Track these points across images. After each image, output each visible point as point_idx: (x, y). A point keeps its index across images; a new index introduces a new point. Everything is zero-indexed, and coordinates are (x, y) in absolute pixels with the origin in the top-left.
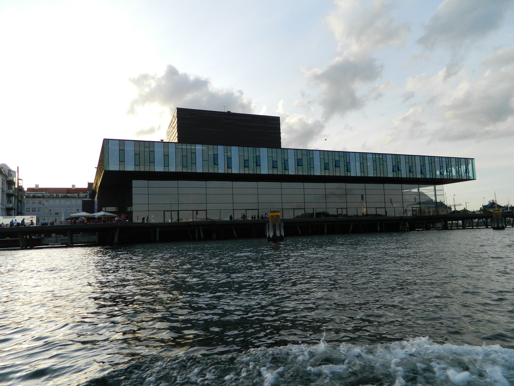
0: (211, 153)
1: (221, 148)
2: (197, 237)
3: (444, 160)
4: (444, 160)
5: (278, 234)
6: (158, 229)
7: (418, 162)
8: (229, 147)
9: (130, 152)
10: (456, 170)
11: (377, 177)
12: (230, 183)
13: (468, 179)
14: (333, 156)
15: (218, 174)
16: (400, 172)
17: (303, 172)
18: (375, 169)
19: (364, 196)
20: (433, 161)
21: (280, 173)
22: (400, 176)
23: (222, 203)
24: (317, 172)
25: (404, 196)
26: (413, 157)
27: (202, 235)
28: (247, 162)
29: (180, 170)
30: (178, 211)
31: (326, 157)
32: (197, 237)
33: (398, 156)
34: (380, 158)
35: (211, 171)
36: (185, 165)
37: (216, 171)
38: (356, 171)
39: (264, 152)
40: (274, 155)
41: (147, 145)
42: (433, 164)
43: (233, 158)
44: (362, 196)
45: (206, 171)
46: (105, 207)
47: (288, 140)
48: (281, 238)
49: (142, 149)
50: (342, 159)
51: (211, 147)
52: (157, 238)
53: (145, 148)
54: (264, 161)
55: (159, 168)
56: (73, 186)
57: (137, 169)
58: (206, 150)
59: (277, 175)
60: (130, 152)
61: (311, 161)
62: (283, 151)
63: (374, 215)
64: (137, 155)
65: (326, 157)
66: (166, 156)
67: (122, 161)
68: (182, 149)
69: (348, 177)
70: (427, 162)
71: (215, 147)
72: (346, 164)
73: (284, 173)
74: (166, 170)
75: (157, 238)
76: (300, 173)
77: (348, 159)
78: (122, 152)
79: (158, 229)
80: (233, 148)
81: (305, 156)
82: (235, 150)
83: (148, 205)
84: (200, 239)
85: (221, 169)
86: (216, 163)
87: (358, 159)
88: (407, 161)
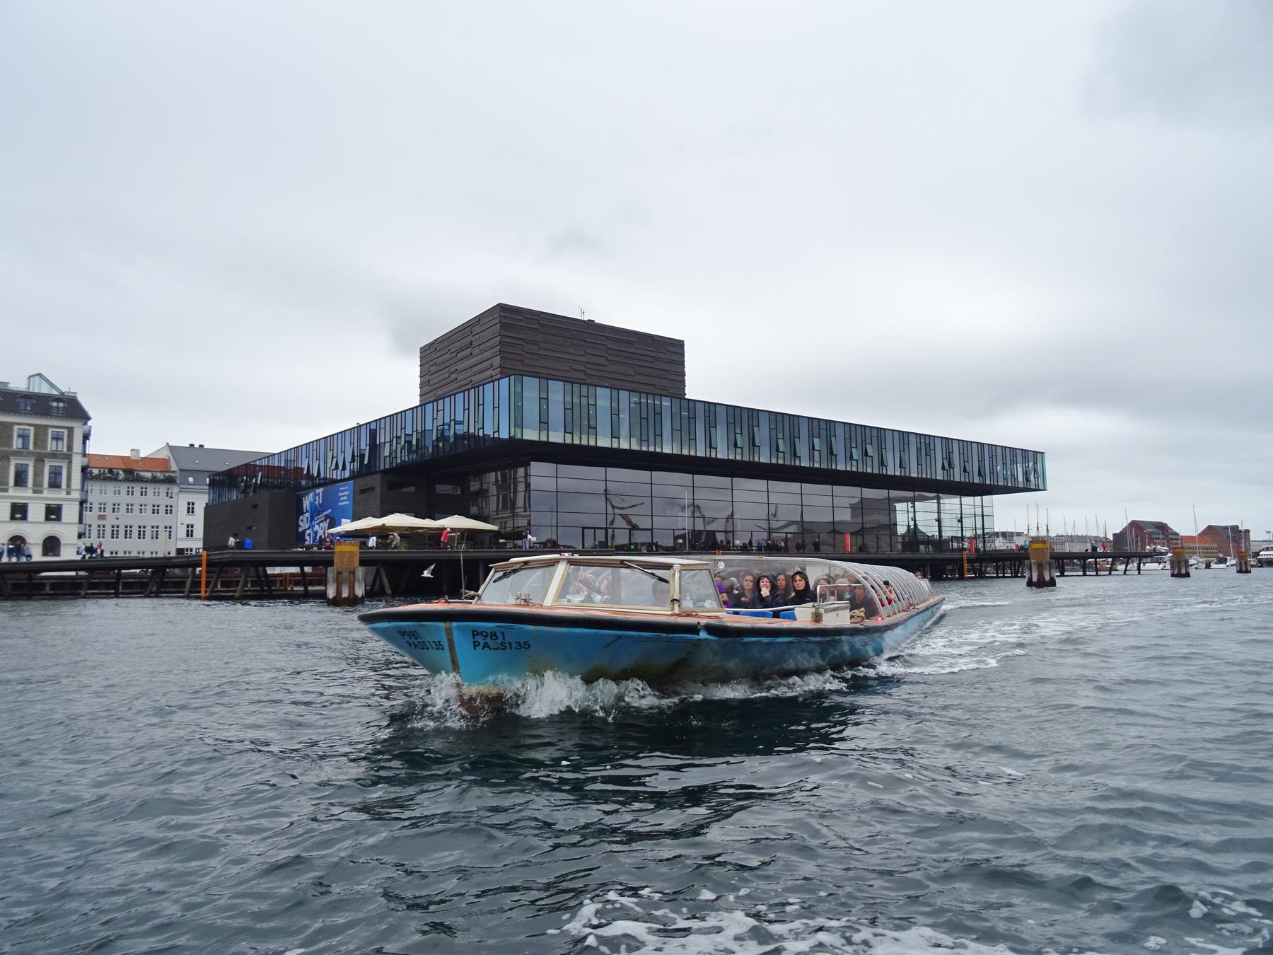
47: (698, 387)
67: (544, 423)
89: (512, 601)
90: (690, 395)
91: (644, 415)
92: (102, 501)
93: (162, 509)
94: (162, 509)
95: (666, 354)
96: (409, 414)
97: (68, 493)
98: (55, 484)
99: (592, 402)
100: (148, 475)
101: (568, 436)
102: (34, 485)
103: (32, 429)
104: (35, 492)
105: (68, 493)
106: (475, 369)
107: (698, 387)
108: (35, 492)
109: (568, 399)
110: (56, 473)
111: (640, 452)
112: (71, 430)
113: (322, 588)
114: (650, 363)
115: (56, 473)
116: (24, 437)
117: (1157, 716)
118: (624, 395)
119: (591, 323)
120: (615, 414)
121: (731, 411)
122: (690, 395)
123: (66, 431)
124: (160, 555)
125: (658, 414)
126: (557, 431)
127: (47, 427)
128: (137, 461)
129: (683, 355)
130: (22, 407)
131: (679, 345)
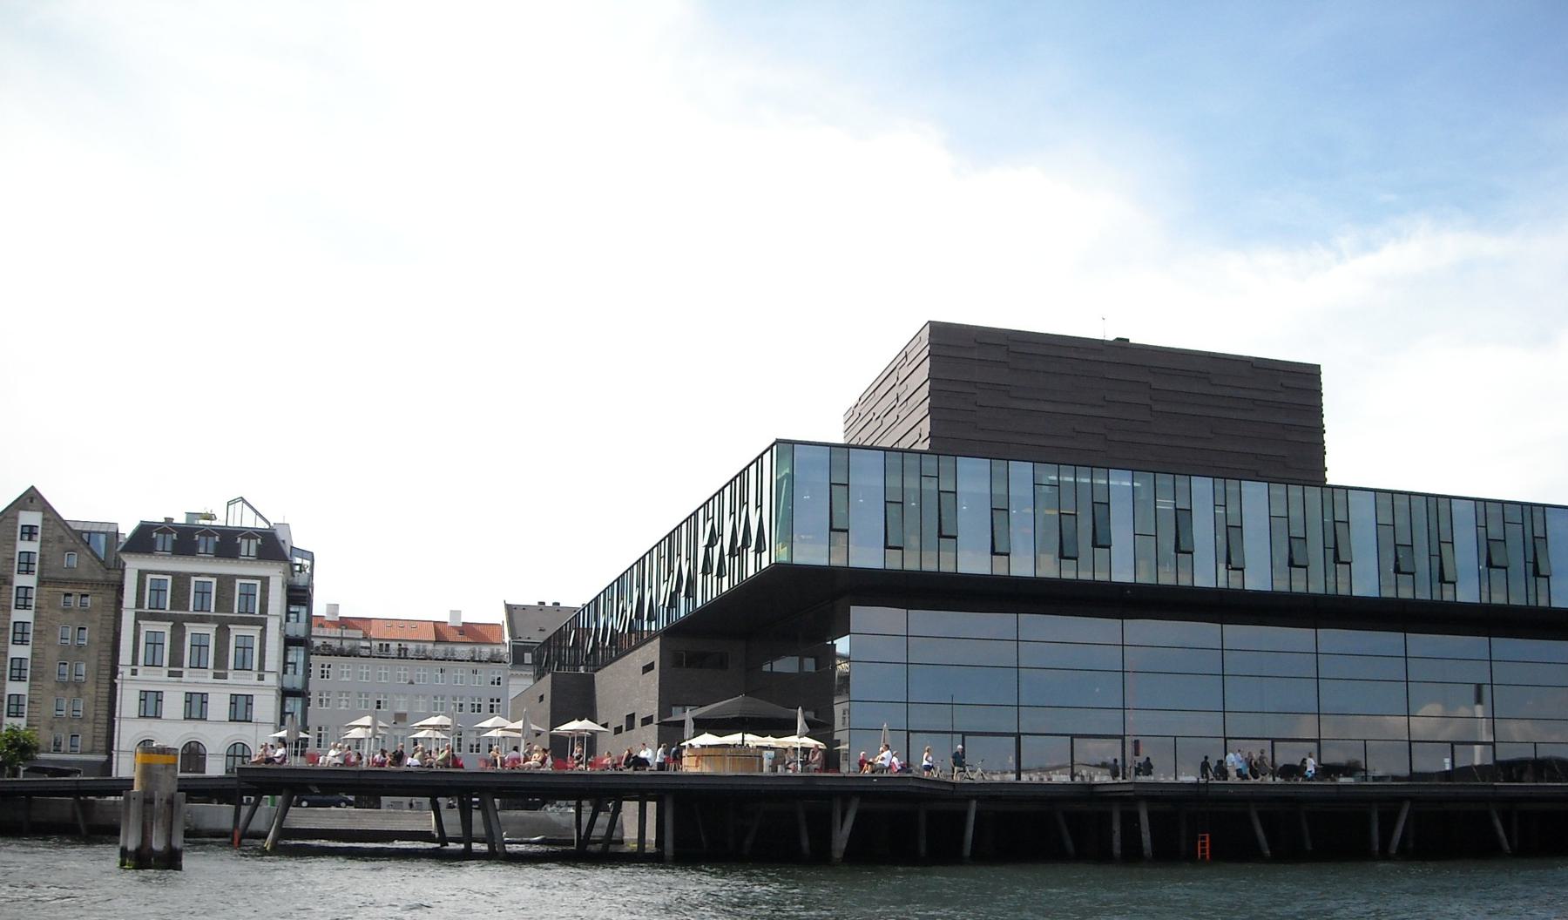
0: (1166, 505)
1: (1202, 486)
8: (1232, 485)
12: (1308, 633)
15: (1193, 590)
16: (1542, 582)
17: (1510, 593)
19: (1486, 690)
21: (1423, 595)
22: (1543, 602)
24: (1365, 581)
27: (1146, 837)
29: (1049, 569)
30: (1018, 736)
31: (1402, 521)
35: (1167, 579)
37: (1184, 581)
39: (1255, 497)
44: (1479, 687)
45: (1145, 578)
47: (1357, 453)
50: (1514, 532)
51: (1165, 481)
54: (1240, 532)
55: (973, 561)
56: (455, 614)
57: (894, 562)
58: (1145, 495)
59: (1413, 603)
61: (1440, 545)
62: (1327, 496)
63: (1446, 775)
65: (1402, 521)
67: (837, 529)
68: (1058, 485)
71: (1182, 482)
72: (1435, 551)
73: (1436, 597)
74: (1000, 570)
76: (1499, 599)
81: (1419, 518)
85: (1206, 574)
86: (1183, 548)
89: (482, 765)
97: (261, 678)
98: (242, 666)
99: (1220, 511)
101: (894, 555)
102: (216, 666)
103: (169, 578)
104: (216, 676)
105: (261, 678)
108: (216, 676)
109: (894, 482)
110: (244, 648)
111: (1060, 583)
112: (265, 581)
113: (1117, 850)
115: (244, 648)
116: (203, 592)
118: (1021, 471)
119: (1122, 343)
120: (999, 511)
123: (258, 583)
125: (1100, 511)
127: (234, 577)
130: (244, 551)
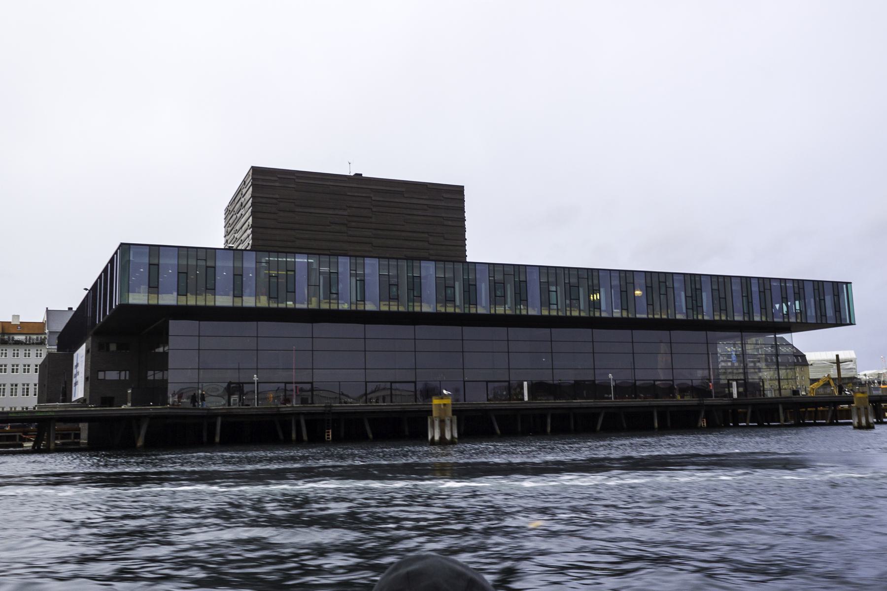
1: (344, 263)
2: (294, 436)
3: (721, 280)
4: (721, 280)
5: (448, 436)
6: (219, 421)
7: (736, 287)
9: (169, 268)
10: (826, 303)
11: (714, 321)
13: (851, 324)
14: (567, 276)
18: (763, 306)
20: (768, 287)
23: (344, 371)
25: (842, 366)
26: (820, 284)
28: (394, 289)
32: (294, 436)
33: (595, 274)
34: (658, 283)
35: (325, 306)
36: (274, 294)
38: (607, 305)
39: (429, 271)
40: (449, 275)
41: (202, 255)
42: (768, 293)
43: (361, 281)
46: (104, 371)
47: (484, 244)
48: (452, 442)
49: (192, 262)
52: (217, 439)
53: (195, 262)
58: (315, 266)
60: (169, 268)
64: (183, 274)
66: (238, 276)
69: (698, 320)
70: (755, 288)
75: (217, 439)
77: (596, 282)
78: (154, 269)
79: (219, 421)
80: (342, 260)
82: (372, 268)
83: (191, 369)
84: (299, 442)
87: (616, 282)
88: (715, 287)
90: (472, 256)
91: (722, 295)
92: (27, 363)
93: (21, 368)
94: (21, 368)
95: (439, 208)
96: (811, 318)
100: (22, 338)
106: (404, 234)
107: (484, 244)
114: (429, 214)
117: (143, 517)
121: (714, 279)
122: (472, 256)
124: (19, 409)
126: (250, 296)
128: (16, 325)
129: (463, 201)
131: (457, 192)
